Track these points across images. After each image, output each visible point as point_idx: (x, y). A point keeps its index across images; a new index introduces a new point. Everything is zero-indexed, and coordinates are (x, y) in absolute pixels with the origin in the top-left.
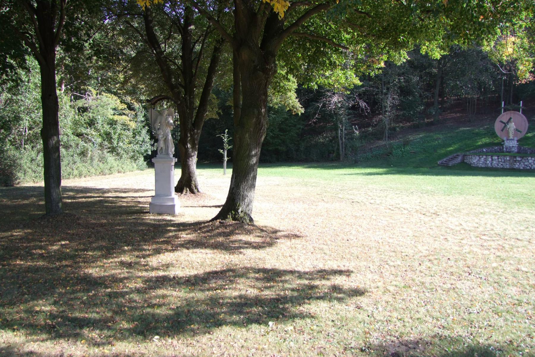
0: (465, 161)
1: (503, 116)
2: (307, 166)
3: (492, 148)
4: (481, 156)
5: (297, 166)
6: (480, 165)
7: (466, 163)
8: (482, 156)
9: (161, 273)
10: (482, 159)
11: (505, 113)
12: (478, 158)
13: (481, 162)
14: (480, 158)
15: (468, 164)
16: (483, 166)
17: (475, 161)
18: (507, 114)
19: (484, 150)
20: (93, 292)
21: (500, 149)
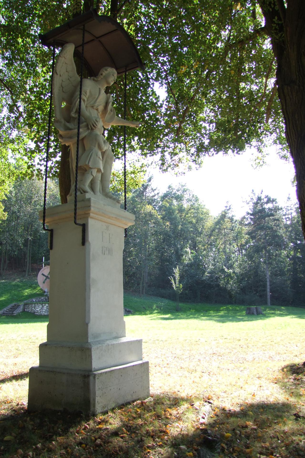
0: (26, 310)
1: (44, 269)
2: (294, 316)
3: (40, 298)
4: (44, 305)
5: (301, 307)
6: (43, 313)
7: (28, 312)
8: (45, 304)
9: (73, 187)
10: (45, 307)
11: (46, 267)
12: (41, 306)
13: (44, 310)
14: (43, 306)
15: (31, 313)
16: (45, 314)
17: (38, 309)
18: (47, 268)
19: (34, 300)
20: (279, 111)
21: (46, 299)
